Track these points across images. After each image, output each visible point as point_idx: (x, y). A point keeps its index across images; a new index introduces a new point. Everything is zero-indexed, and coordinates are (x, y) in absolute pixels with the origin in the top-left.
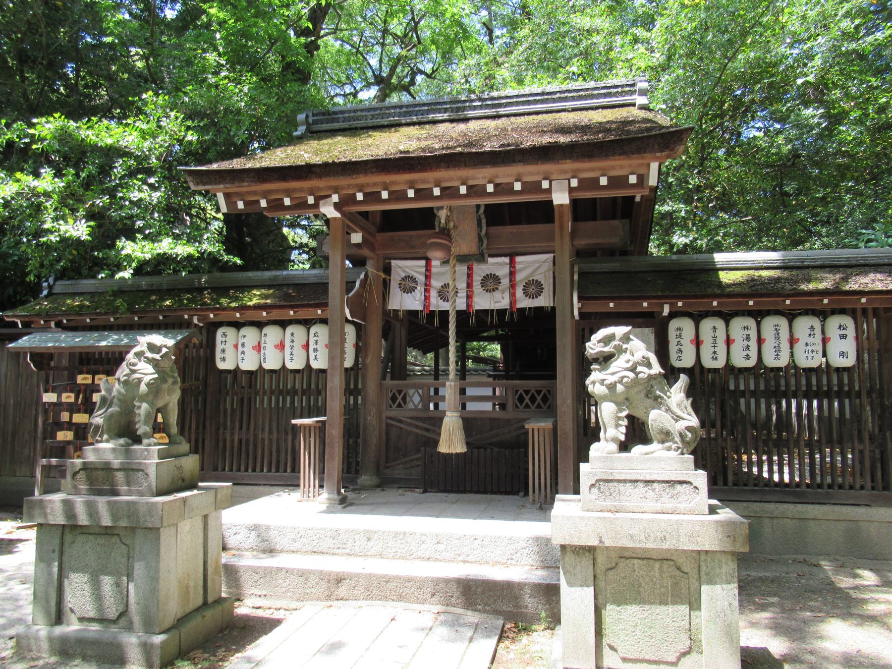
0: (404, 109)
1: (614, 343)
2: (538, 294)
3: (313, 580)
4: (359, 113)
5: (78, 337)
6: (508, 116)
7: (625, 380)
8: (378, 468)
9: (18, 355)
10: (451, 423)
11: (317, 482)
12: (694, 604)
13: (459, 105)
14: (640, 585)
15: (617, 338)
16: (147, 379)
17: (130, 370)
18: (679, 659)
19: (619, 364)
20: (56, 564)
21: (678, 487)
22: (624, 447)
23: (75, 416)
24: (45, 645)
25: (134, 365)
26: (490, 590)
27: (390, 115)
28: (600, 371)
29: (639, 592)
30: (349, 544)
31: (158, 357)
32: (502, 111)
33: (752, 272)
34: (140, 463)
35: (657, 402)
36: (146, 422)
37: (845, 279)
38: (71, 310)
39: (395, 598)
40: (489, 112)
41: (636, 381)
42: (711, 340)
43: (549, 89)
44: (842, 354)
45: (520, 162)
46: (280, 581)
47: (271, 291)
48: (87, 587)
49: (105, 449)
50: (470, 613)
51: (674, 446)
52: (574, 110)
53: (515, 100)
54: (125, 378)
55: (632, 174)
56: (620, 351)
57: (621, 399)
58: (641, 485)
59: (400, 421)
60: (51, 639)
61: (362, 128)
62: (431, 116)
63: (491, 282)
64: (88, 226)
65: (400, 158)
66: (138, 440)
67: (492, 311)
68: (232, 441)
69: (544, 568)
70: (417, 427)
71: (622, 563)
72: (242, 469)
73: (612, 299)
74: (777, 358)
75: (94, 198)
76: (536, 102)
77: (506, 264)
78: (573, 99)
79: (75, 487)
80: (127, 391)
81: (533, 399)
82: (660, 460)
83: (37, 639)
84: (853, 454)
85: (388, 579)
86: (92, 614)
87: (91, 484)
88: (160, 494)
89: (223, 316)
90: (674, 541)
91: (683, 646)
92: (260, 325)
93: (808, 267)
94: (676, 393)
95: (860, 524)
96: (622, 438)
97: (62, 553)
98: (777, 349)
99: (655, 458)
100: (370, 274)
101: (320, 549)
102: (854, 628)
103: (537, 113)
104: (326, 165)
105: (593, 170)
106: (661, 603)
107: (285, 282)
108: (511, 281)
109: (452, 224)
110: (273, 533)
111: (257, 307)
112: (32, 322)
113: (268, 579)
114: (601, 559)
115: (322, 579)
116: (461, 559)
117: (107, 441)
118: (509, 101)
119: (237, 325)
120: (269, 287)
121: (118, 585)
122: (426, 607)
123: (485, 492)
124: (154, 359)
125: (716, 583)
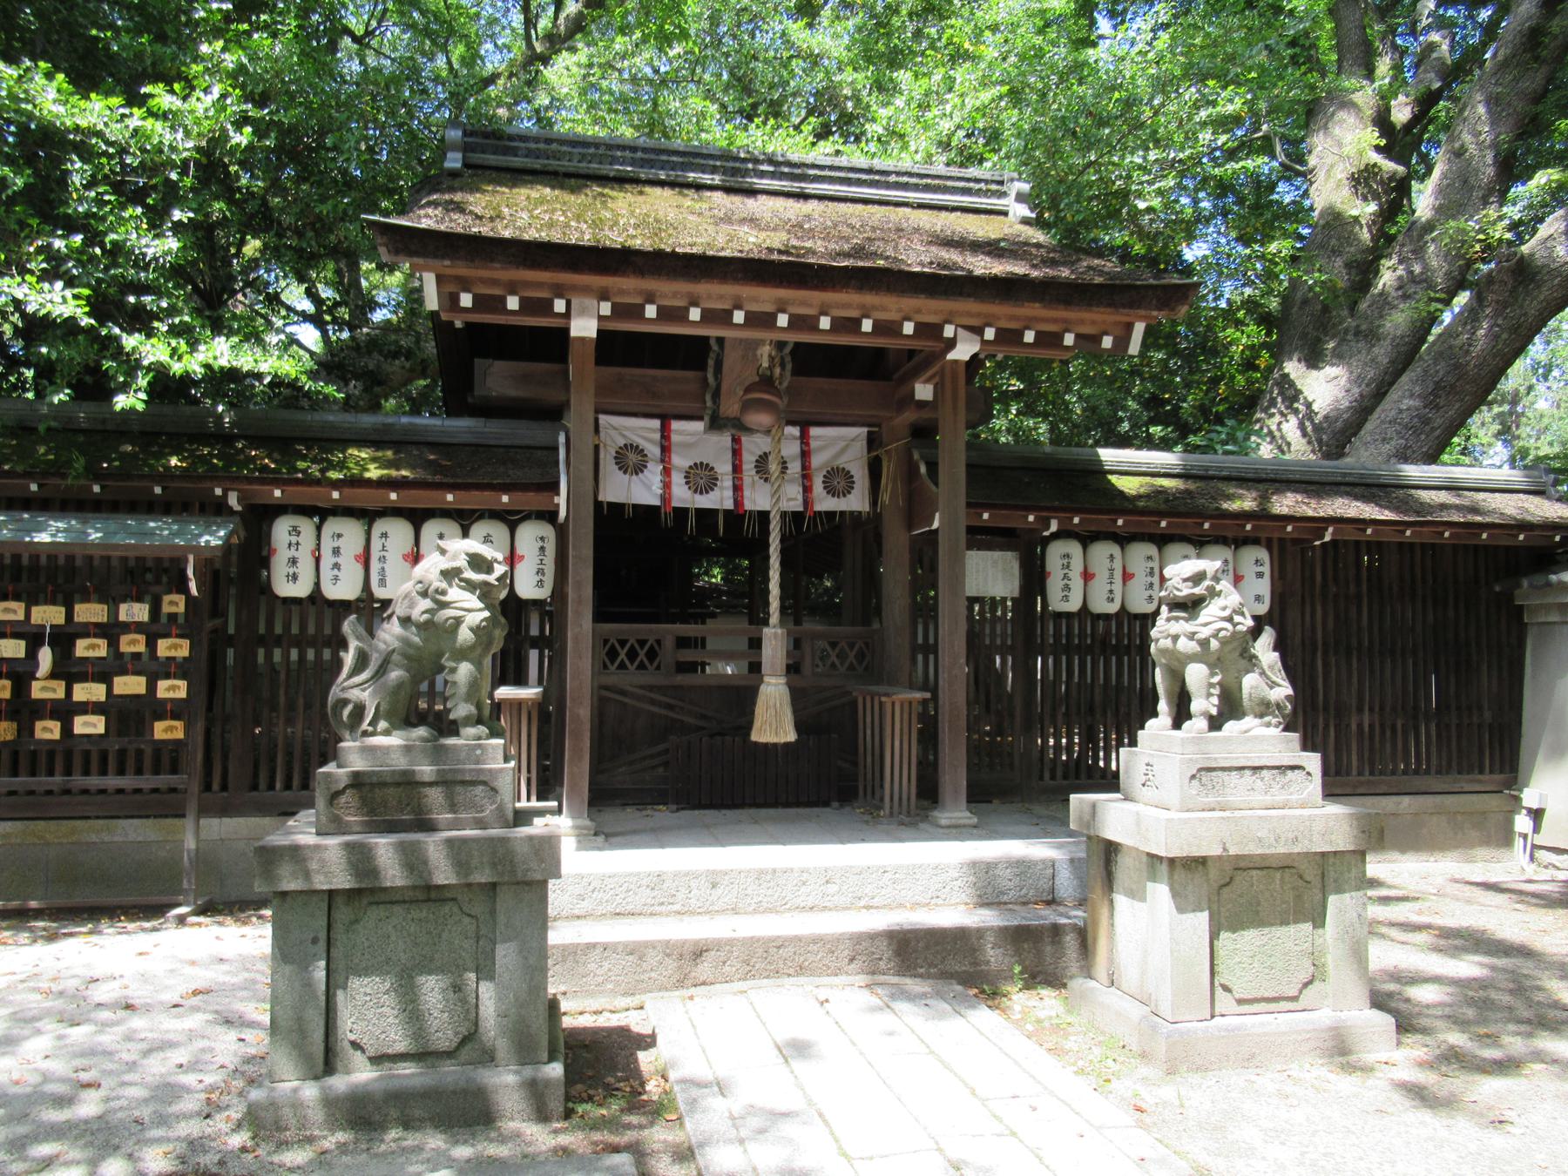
0: (639, 154)
1: (1207, 583)
3: (653, 958)
6: (821, 198)
7: (1222, 634)
10: (774, 692)
12: (1319, 920)
13: (737, 165)
14: (1258, 904)
17: (436, 601)
19: (1211, 612)
20: (323, 963)
21: (1289, 773)
22: (1215, 723)
24: (317, 1115)
25: (444, 593)
26: (937, 944)
27: (614, 160)
28: (1187, 620)
29: (1257, 912)
30: (680, 896)
31: (492, 578)
32: (812, 188)
33: (1148, 479)
39: (791, 971)
40: (785, 185)
42: (1107, 574)
43: (878, 163)
45: (969, 296)
46: (592, 966)
48: (389, 1000)
52: (921, 206)
54: (426, 616)
56: (1213, 593)
57: (1212, 659)
58: (1248, 772)
59: (623, 693)
62: (692, 176)
64: (76, 297)
66: (453, 729)
68: (1360, 726)
70: (653, 702)
71: (1239, 877)
72: (296, 782)
74: (1066, 599)
76: (860, 183)
77: (795, 438)
78: (916, 188)
80: (425, 641)
81: (632, 655)
83: (297, 1105)
85: (780, 943)
86: (401, 1046)
87: (372, 812)
91: (1304, 976)
92: (368, 516)
93: (1212, 478)
96: (1214, 711)
97: (329, 943)
99: (1256, 737)
101: (629, 908)
103: (866, 201)
104: (658, 255)
105: (1055, 321)
106: (1282, 924)
107: (415, 438)
113: (568, 964)
115: (668, 955)
116: (862, 903)
117: (387, 733)
119: (321, 513)
121: (457, 988)
122: (842, 979)
124: (486, 584)
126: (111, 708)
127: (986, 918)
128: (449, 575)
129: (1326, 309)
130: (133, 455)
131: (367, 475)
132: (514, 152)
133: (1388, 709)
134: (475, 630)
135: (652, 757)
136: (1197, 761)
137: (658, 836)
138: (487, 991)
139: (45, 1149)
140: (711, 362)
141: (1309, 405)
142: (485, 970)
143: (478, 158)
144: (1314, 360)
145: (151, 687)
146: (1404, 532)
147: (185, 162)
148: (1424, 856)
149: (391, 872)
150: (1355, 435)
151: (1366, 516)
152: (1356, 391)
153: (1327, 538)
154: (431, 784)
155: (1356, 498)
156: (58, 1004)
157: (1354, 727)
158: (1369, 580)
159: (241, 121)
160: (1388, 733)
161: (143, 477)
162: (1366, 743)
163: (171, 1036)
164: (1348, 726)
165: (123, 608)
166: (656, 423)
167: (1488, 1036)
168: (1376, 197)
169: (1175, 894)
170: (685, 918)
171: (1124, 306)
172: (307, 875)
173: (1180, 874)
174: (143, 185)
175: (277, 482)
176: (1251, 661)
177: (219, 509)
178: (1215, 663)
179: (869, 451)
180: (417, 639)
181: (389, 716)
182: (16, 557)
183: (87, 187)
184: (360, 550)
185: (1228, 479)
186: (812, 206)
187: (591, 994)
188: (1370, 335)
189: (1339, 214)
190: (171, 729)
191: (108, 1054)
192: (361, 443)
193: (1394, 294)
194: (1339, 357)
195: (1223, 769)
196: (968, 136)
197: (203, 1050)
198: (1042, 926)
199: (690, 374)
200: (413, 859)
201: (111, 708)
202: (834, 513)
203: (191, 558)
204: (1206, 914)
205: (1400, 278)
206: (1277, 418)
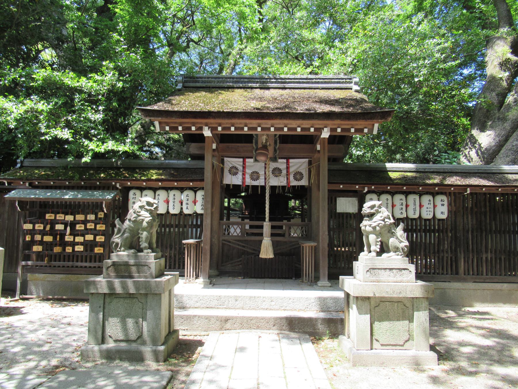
0: (235, 80)
2: (301, 179)
3: (213, 321)
4: (210, 79)
5: (49, 193)
6: (290, 88)
7: (380, 225)
8: (218, 266)
9: (12, 201)
10: (267, 243)
11: (194, 273)
12: (411, 320)
15: (377, 206)
16: (147, 220)
17: (137, 215)
18: (404, 343)
19: (377, 218)
20: (102, 313)
21: (403, 271)
23: (45, 237)
24: (98, 354)
25: (139, 212)
26: (302, 322)
27: (227, 82)
28: (369, 221)
29: (388, 316)
30: (226, 303)
31: (152, 208)
32: (287, 85)
33: (403, 173)
34: (146, 262)
35: (393, 234)
36: (146, 242)
37: (444, 179)
38: (40, 178)
41: (385, 225)
44: (442, 213)
45: (316, 119)
46: (195, 322)
47: (161, 171)
48: (119, 325)
49: (123, 255)
50: (292, 333)
51: (400, 254)
53: (293, 80)
55: (366, 128)
56: (378, 212)
57: (378, 233)
59: (230, 242)
60: (101, 351)
61: (213, 88)
63: (277, 172)
64: (70, 133)
65: (255, 113)
66: (141, 251)
67: (279, 186)
69: (322, 311)
70: (239, 245)
71: (382, 304)
73: (341, 184)
74: (415, 214)
75: (66, 115)
76: (303, 83)
78: (322, 83)
79: (108, 274)
80: (134, 225)
82: (395, 259)
83: (93, 351)
84: (434, 259)
86: (122, 338)
88: (156, 277)
89: (135, 184)
90: (404, 294)
91: (406, 338)
93: (427, 172)
94: (399, 231)
95: (446, 290)
96: (378, 250)
97: (104, 308)
98: (415, 210)
99: (393, 259)
100: (215, 165)
101: (211, 306)
102: (457, 332)
103: (305, 88)
105: (348, 125)
106: (397, 320)
108: (287, 172)
109: (268, 143)
110: (185, 299)
111: (157, 180)
112: (12, 183)
113: (188, 321)
114: (373, 302)
117: (124, 251)
118: (290, 81)
120: (159, 169)
121: (137, 323)
122: (271, 331)
123: (275, 278)
124: (151, 210)
125: (420, 311)
127: (322, 315)
128: (141, 207)
129: (488, 111)
130: (93, 174)
131: (152, 178)
132: (198, 82)
133: (498, 252)
134: (148, 223)
135: (238, 262)
136: (369, 266)
137: (229, 286)
138: (145, 324)
139: (31, 357)
140: (254, 141)
141: (480, 145)
142: (144, 319)
143: (187, 85)
144: (483, 129)
145: (95, 238)
146: (514, 190)
147: (104, 93)
148: (514, 306)
149: (118, 289)
150: (497, 155)
151: (481, 184)
152: (497, 139)
153: (468, 192)
154: (133, 265)
155: (481, 178)
156: (53, 322)
157: (484, 258)
158: (490, 206)
159: (119, 80)
160: (498, 261)
161: (94, 180)
162: (489, 264)
163: (76, 333)
164: (482, 258)
165: (88, 216)
166: (241, 160)
167: (475, 364)
168: (509, 70)
169: (358, 308)
170: (227, 310)
171: (369, 119)
172: (97, 289)
173: (360, 302)
174: (92, 100)
175: (129, 180)
176: (393, 234)
177: (115, 188)
178: (379, 234)
179: (309, 166)
180: (132, 225)
181: (124, 246)
182: (53, 202)
183: (79, 102)
184: (193, 200)
185: (433, 172)
186: (287, 91)
187: (194, 330)
188: (504, 119)
189: (494, 77)
190: (99, 250)
191: (57, 335)
192: (154, 168)
193: (513, 104)
194: (492, 127)
195: (379, 269)
196: (358, 62)
197: (82, 337)
198: (337, 319)
199: (248, 144)
200: (124, 286)
201: (85, 244)
202: (295, 186)
203: (104, 202)
204: (369, 316)
205: (515, 99)
206: (468, 150)
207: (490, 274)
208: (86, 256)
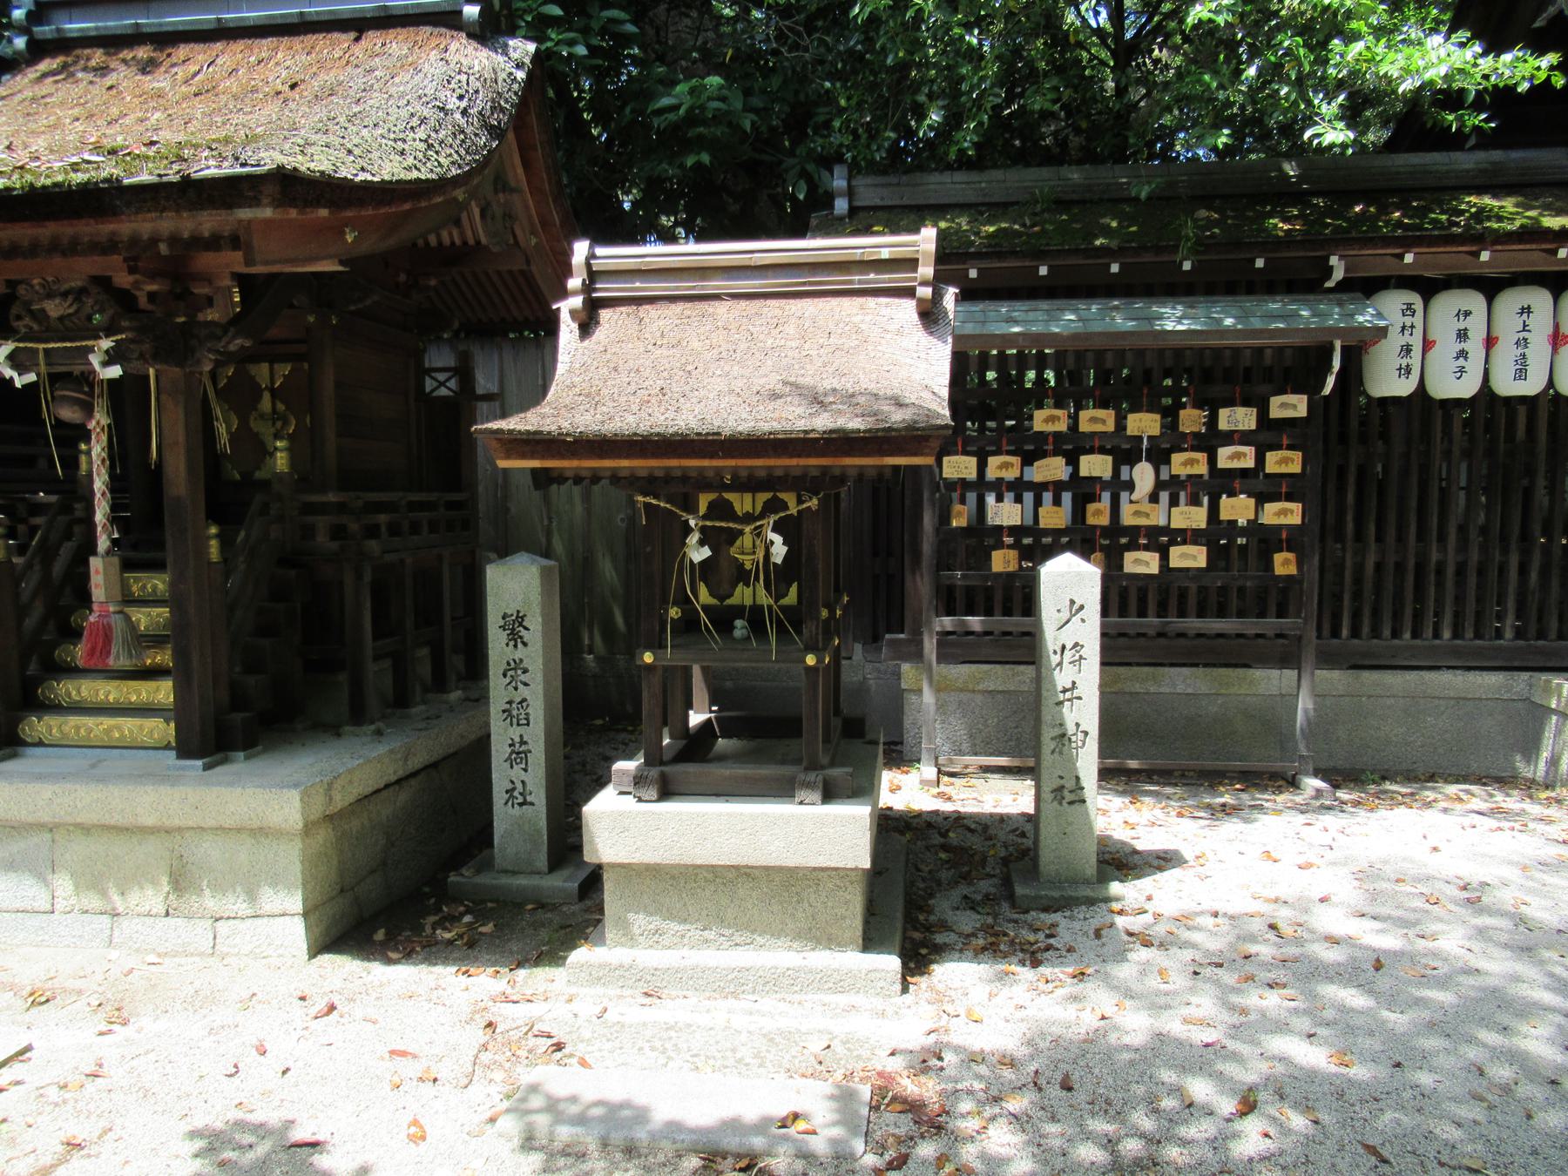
68: (1359, 569)
72: (1366, 629)
74: (1521, 374)
126: (1215, 535)
165: (1224, 413)
175: (1407, 243)
203: (1338, 344)
207: (1469, 634)
208: (1223, 591)
